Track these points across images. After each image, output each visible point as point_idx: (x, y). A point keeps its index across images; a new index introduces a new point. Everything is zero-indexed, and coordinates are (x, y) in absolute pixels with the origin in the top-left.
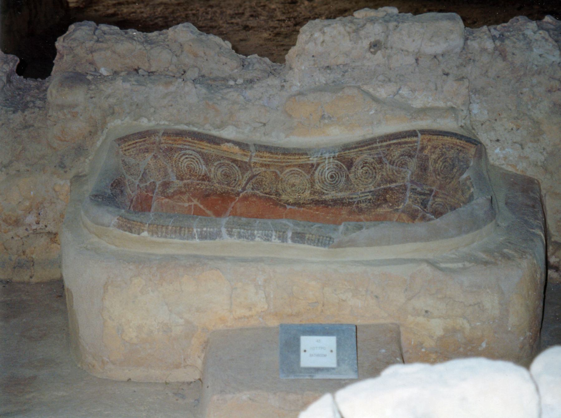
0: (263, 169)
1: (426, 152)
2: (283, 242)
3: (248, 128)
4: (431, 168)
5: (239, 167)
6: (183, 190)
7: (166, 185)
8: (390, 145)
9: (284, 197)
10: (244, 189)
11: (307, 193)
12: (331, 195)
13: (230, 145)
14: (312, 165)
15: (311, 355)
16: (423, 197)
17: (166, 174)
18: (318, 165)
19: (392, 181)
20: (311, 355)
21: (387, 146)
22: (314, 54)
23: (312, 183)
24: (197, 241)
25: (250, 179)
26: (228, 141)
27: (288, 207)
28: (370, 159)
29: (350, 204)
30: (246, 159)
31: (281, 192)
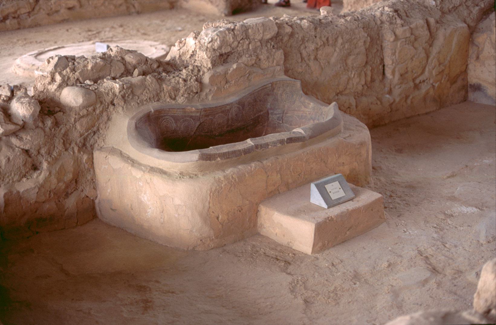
0: (206, 118)
1: (275, 91)
14: (228, 110)
16: (278, 116)
18: (230, 109)
19: (261, 111)
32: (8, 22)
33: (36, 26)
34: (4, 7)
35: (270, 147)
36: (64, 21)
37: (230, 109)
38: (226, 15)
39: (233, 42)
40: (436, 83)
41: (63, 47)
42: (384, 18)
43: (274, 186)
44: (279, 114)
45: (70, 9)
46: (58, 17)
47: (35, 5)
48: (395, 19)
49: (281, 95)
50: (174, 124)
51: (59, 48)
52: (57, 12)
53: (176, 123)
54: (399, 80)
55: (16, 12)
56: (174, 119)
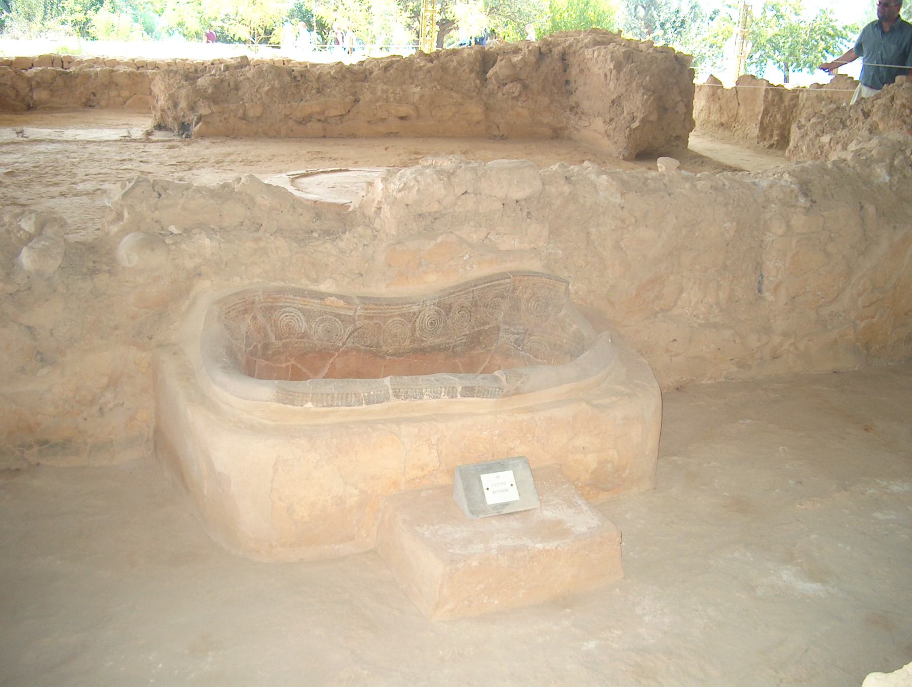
0: (367, 321)
1: (517, 293)
2: (452, 397)
3: (347, 280)
4: (523, 307)
5: (342, 321)
6: (282, 350)
7: (266, 347)
8: (484, 288)
9: (384, 348)
10: (344, 344)
11: (408, 342)
12: (430, 341)
13: (333, 299)
14: (415, 314)
15: (494, 492)
16: (516, 336)
17: (266, 336)
18: (420, 312)
19: (485, 323)
20: (494, 492)
21: (482, 289)
22: (409, 202)
23: (413, 330)
24: (364, 406)
25: (353, 332)
26: (331, 295)
27: (388, 358)
28: (467, 304)
29: (446, 349)
30: (351, 313)
31: (381, 343)
32: (309, 125)
33: (351, 136)
34: (307, 103)
35: (425, 397)
36: (389, 135)
37: (420, 312)
38: (625, 159)
39: (446, 196)
40: (862, 321)
41: (347, 170)
42: (774, 193)
43: (423, 470)
44: (518, 334)
45: (402, 118)
46: (381, 128)
47: (353, 107)
48: (796, 196)
49: (528, 302)
50: (304, 324)
51: (340, 171)
52: (383, 120)
53: (308, 321)
54: (786, 304)
55: (323, 113)
56: (304, 315)
